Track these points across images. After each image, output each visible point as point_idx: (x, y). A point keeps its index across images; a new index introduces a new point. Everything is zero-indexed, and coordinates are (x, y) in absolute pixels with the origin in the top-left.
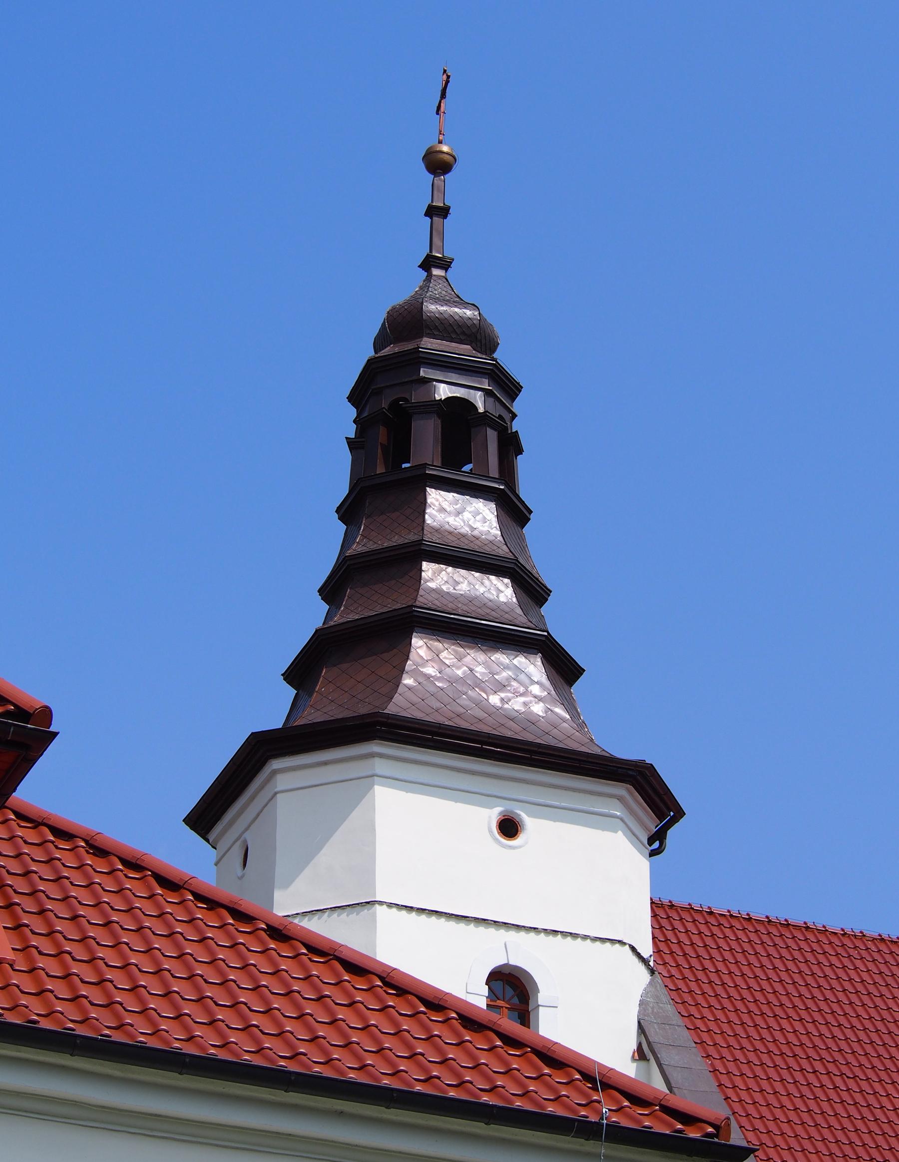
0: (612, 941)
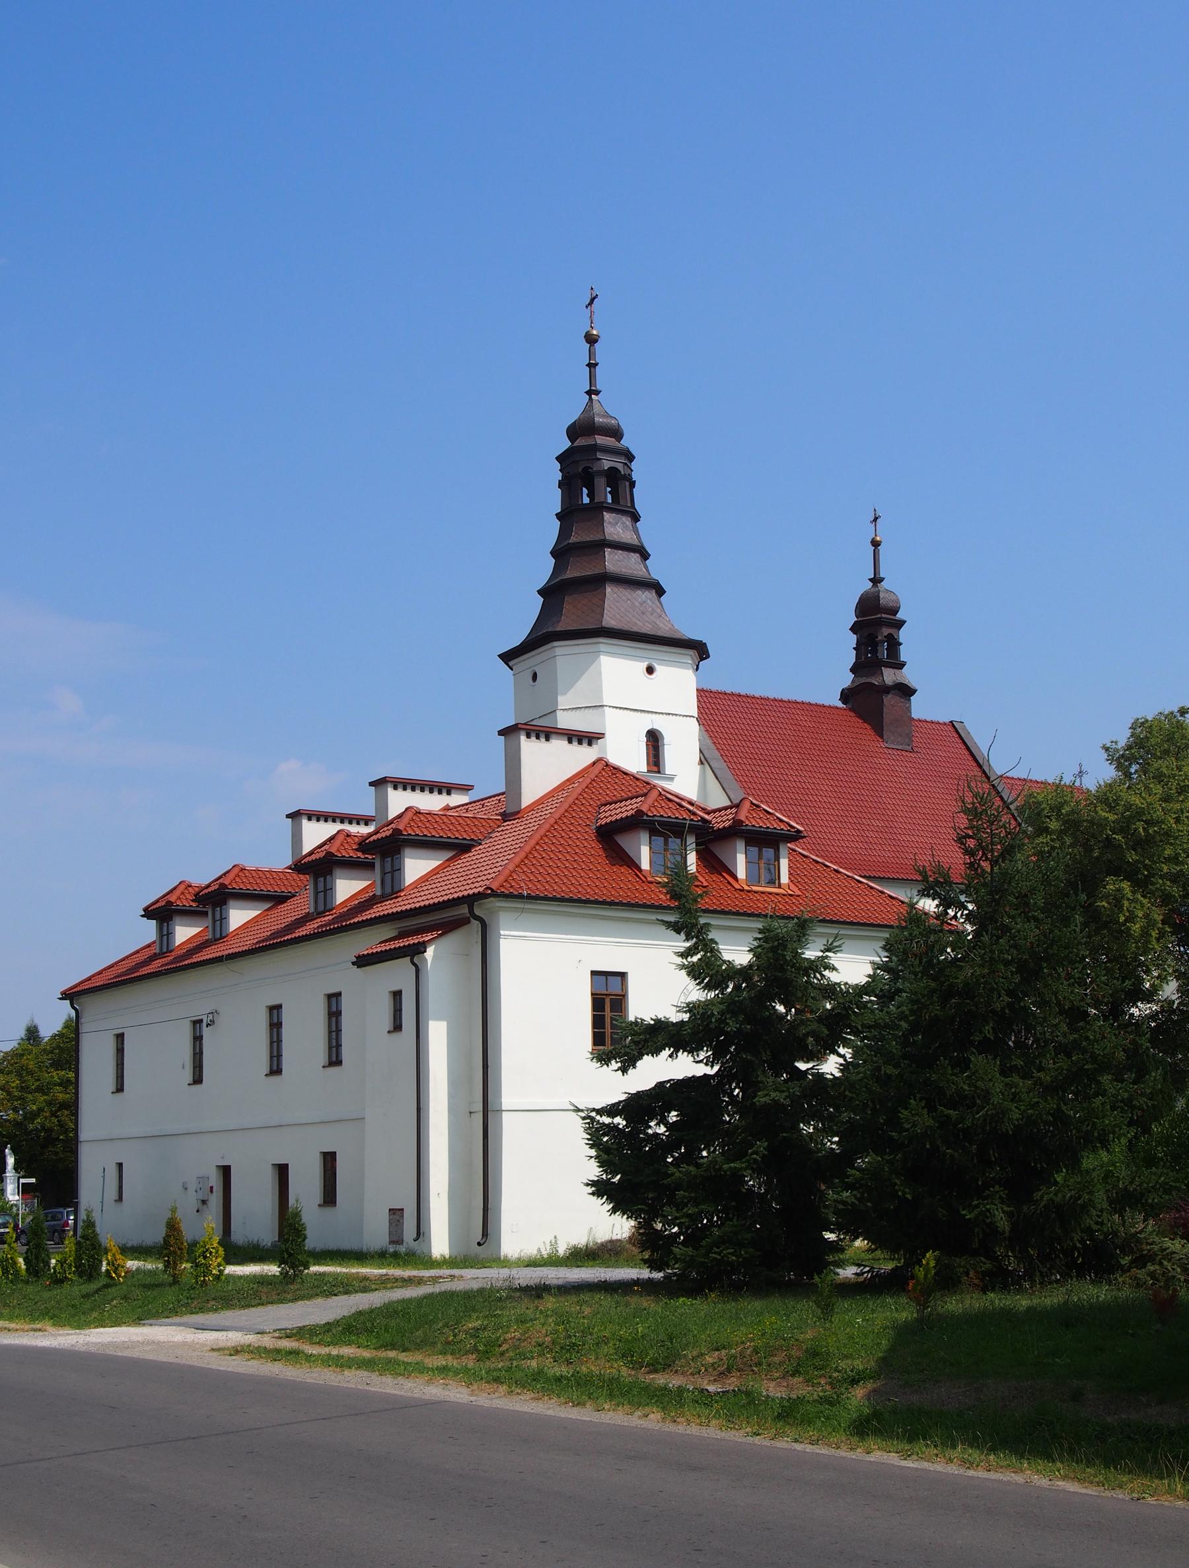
0: (690, 716)
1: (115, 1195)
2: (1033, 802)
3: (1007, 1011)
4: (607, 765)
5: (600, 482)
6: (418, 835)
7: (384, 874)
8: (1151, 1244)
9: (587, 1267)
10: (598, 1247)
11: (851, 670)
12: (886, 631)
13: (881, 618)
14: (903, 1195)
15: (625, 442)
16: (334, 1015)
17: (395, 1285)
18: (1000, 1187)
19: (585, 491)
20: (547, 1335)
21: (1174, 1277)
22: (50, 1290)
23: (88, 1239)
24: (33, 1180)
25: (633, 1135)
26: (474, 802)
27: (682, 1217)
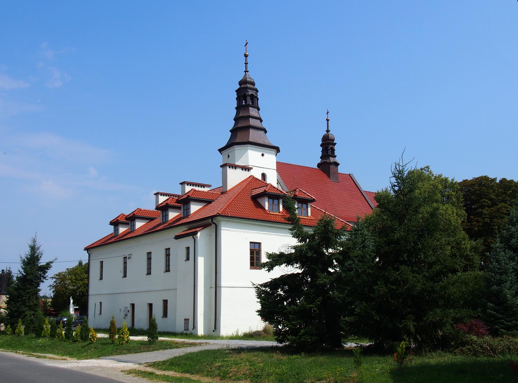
1: (99, 312)
2: (379, 195)
3: (412, 249)
4: (254, 178)
5: (248, 98)
6: (195, 197)
7: (184, 210)
8: (466, 338)
9: (250, 340)
10: (253, 333)
11: (321, 158)
12: (331, 146)
13: (329, 142)
14: (376, 318)
15: (256, 86)
16: (168, 255)
17: (187, 346)
18: (412, 315)
19: (244, 101)
20: (247, 371)
21: (478, 351)
22: (72, 344)
23: (85, 327)
24: (78, 307)
25: (273, 294)
26: (212, 190)
27: (290, 324)
